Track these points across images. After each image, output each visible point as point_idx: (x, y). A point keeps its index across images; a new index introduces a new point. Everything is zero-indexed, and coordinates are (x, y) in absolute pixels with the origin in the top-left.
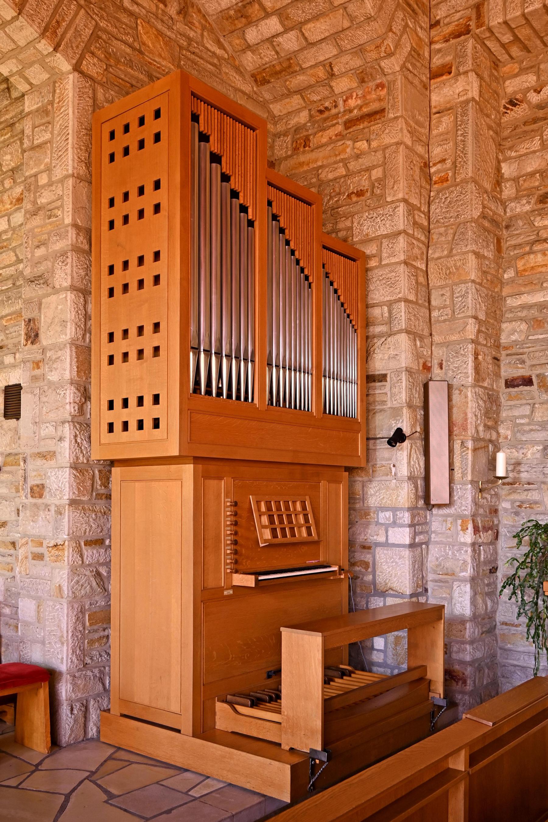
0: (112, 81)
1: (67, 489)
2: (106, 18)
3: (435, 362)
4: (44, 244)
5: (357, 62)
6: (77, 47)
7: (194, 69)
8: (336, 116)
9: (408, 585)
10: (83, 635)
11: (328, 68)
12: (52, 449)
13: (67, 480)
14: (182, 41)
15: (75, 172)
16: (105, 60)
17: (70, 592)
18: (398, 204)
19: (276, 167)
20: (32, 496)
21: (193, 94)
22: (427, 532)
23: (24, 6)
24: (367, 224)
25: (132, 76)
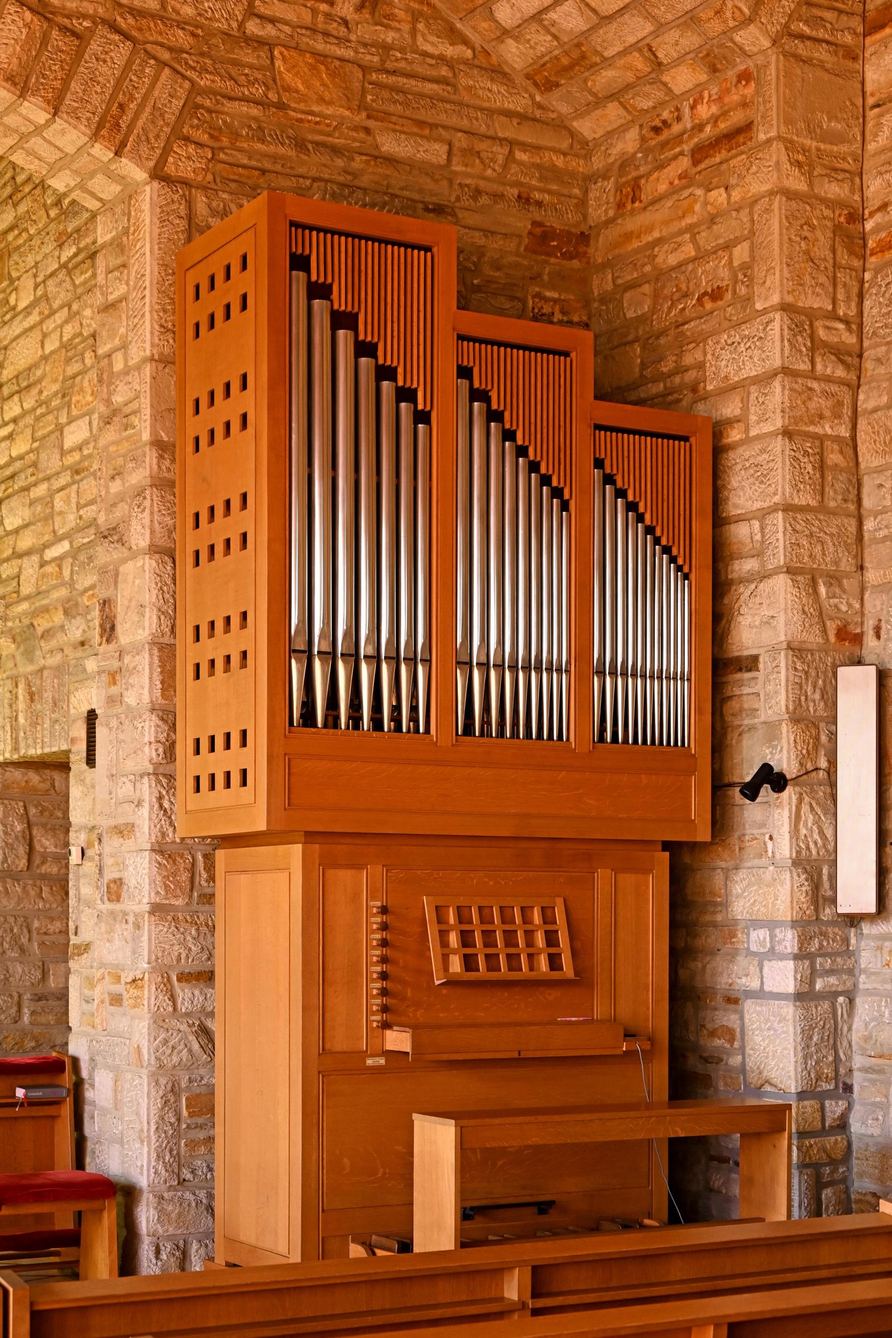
0: (225, 174)
1: (147, 887)
2: (211, 69)
3: (870, 624)
4: (118, 474)
5: (691, 40)
6: (157, 137)
7: (395, 102)
8: (679, 139)
9: (792, 1074)
10: (177, 1130)
11: (648, 54)
12: (130, 820)
13: (146, 871)
14: (368, 57)
15: (155, 352)
16: (211, 143)
17: (153, 1058)
18: (771, 315)
19: (592, 243)
20: (109, 899)
21: (293, 224)
22: (851, 972)
23: (63, 99)
24: (726, 355)
25: (266, 155)
